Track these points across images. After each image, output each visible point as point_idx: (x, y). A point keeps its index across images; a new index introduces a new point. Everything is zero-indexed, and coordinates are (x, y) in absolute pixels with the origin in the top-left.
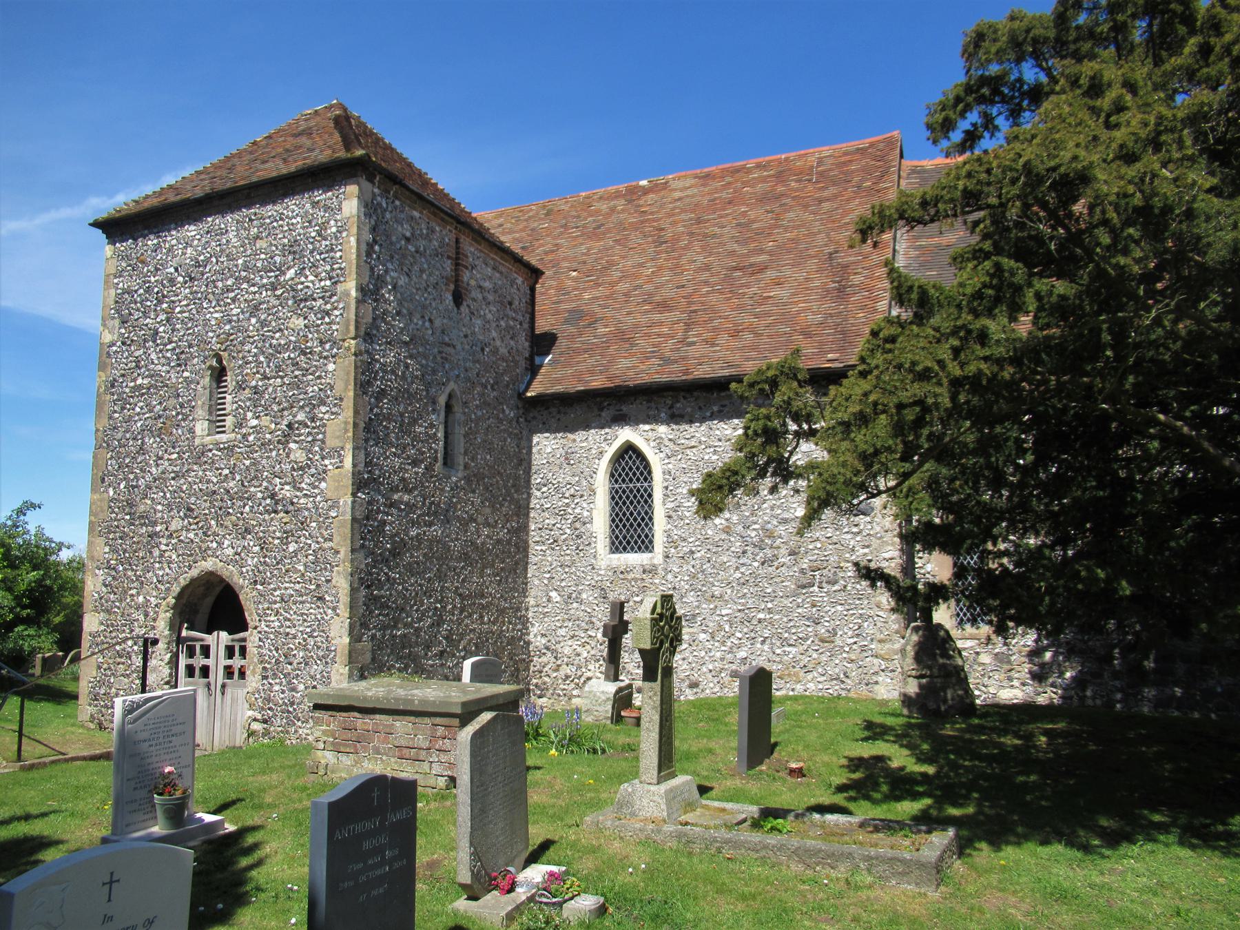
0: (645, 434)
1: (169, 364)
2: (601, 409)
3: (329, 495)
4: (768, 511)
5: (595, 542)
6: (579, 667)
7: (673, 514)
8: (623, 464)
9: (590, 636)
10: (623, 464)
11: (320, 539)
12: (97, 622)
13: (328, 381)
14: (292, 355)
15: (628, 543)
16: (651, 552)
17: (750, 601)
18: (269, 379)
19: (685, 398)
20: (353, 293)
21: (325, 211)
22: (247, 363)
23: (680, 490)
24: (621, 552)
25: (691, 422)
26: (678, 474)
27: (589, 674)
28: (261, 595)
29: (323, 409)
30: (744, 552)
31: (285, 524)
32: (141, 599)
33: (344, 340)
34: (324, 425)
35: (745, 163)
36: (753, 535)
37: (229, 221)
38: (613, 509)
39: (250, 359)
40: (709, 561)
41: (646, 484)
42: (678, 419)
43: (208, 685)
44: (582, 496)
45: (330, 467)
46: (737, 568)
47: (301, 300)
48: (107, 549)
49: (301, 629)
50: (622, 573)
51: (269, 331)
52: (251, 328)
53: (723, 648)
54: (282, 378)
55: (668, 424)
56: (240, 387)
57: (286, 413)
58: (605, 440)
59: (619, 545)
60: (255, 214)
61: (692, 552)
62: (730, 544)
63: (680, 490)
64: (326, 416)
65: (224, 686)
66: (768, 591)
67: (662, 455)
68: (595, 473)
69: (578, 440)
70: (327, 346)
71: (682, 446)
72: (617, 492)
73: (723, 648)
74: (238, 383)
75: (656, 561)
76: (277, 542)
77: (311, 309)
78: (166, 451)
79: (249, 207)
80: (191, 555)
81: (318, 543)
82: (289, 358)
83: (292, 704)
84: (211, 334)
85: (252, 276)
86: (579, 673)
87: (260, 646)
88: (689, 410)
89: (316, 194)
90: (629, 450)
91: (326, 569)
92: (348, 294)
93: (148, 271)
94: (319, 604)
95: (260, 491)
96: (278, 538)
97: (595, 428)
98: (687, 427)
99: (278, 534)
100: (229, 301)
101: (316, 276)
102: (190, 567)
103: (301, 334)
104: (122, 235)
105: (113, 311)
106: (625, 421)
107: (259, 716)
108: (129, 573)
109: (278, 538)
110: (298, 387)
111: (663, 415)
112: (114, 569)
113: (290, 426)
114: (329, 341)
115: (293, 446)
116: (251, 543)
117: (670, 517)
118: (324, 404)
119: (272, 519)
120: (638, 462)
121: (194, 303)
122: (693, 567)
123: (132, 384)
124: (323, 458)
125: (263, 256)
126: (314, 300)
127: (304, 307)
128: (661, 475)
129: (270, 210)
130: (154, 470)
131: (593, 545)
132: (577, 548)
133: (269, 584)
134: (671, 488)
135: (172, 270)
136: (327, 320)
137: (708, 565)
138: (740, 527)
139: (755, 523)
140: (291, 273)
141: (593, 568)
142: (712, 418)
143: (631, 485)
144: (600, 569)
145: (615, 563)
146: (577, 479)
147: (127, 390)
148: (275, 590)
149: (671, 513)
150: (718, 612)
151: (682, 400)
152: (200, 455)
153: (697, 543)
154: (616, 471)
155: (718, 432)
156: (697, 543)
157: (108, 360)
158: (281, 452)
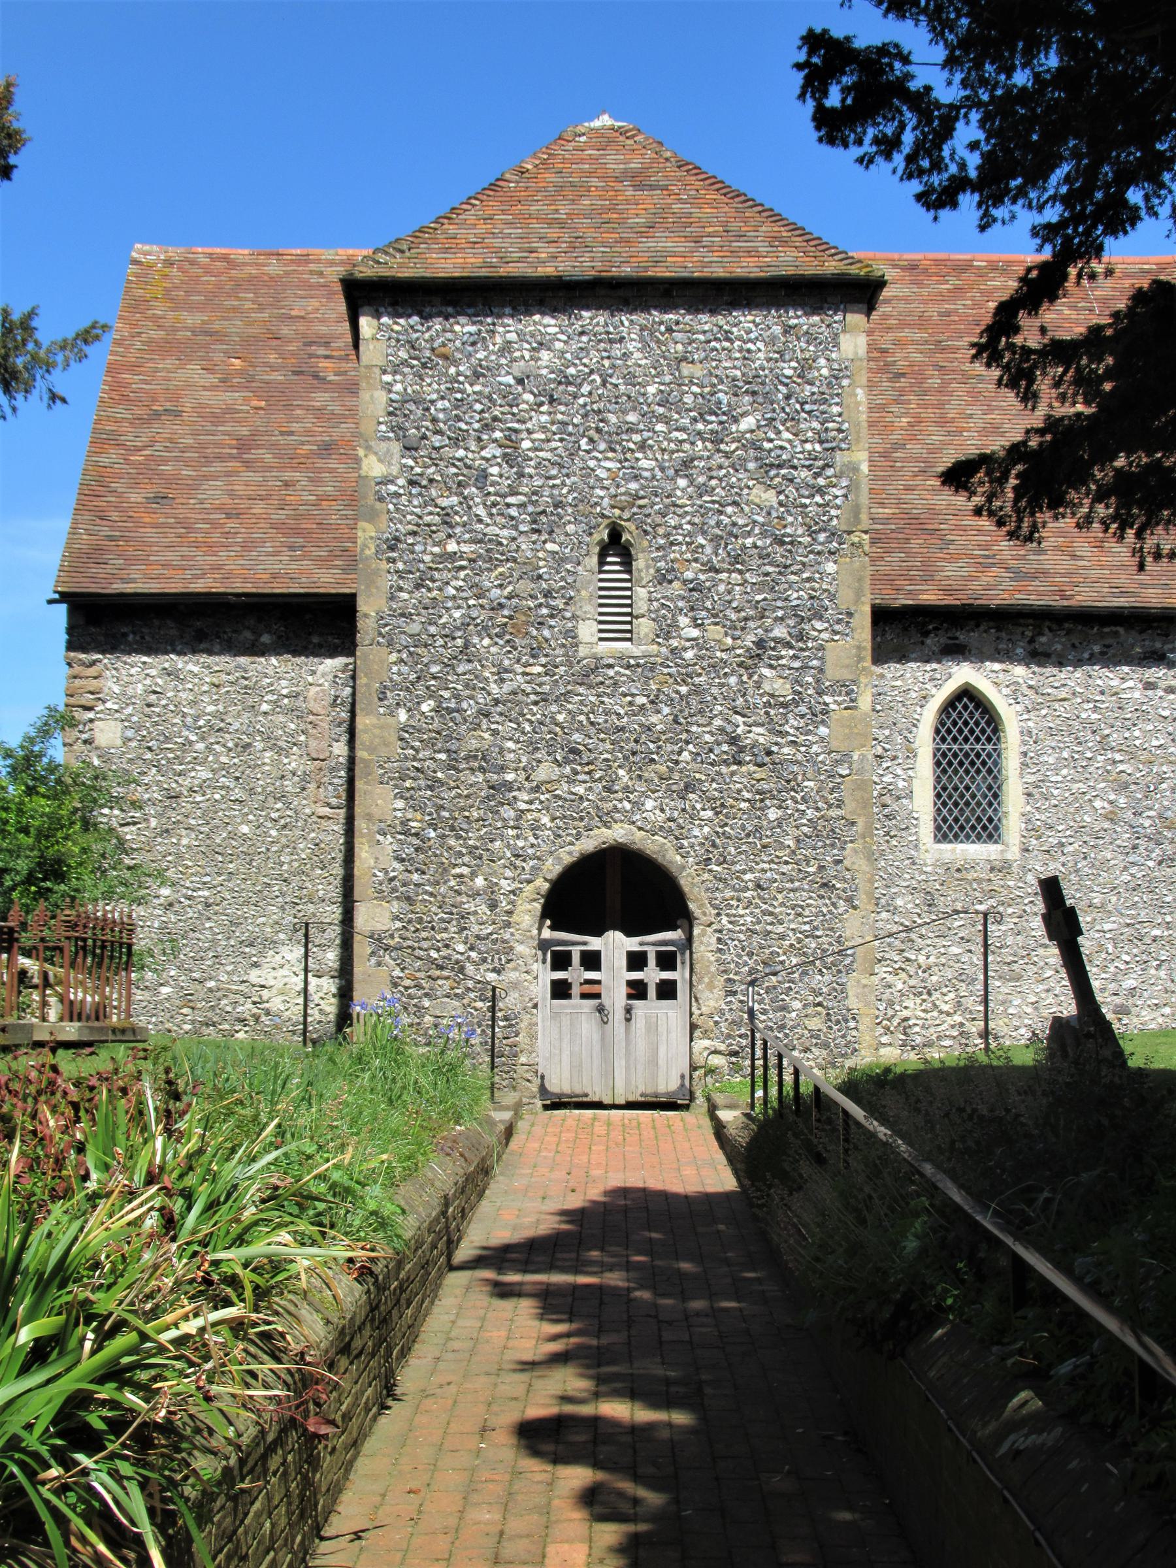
0: (994, 675)
1: (516, 528)
2: (926, 634)
3: (834, 745)
4: (1168, 793)
5: (916, 826)
6: (891, 1004)
7: (1035, 791)
8: (954, 715)
9: (908, 960)
10: (954, 715)
11: (820, 804)
12: (388, 914)
13: (825, 586)
14: (759, 543)
15: (962, 828)
16: (996, 842)
17: (1143, 914)
18: (717, 571)
19: (1051, 630)
20: (865, 468)
21: (808, 343)
22: (672, 544)
23: (1044, 758)
24: (950, 842)
25: (1060, 664)
26: (1041, 735)
27: (905, 1013)
28: (720, 880)
29: (819, 625)
30: (1135, 847)
31: (758, 781)
32: (480, 882)
33: (850, 533)
34: (821, 648)
35: (968, 257)
36: (1147, 825)
37: (628, 323)
38: (938, 780)
39: (680, 538)
40: (1085, 858)
41: (989, 747)
42: (1043, 659)
43: (601, 1009)
44: (895, 758)
45: (833, 707)
46: (1125, 869)
47: (772, 465)
48: (400, 804)
49: (792, 926)
50: (958, 870)
51: (713, 502)
52: (679, 493)
53: (1104, 976)
54: (740, 572)
55: (1027, 665)
56: (662, 579)
57: (751, 624)
58: (932, 679)
59: (946, 831)
60: (677, 323)
61: (1062, 845)
62: (1114, 836)
63: (1044, 758)
64: (825, 636)
65: (628, 1010)
66: (1168, 899)
67: (1019, 708)
68: (915, 726)
69: (889, 676)
70: (822, 537)
71: (1048, 698)
72: (944, 755)
73: (1104, 976)
74: (658, 570)
75: (1009, 856)
76: (744, 805)
77: (791, 481)
78: (518, 661)
79: (665, 309)
80: (582, 819)
81: (817, 809)
82: (755, 546)
83: (782, 1027)
84: (599, 492)
85: (676, 416)
86: (890, 1012)
87: (720, 950)
88: (1059, 647)
89: (791, 313)
90: (967, 695)
91: (833, 845)
92: (856, 469)
93: (459, 374)
94: (822, 892)
95: (710, 733)
96: (748, 800)
97: (916, 660)
98: (1055, 671)
99: (747, 795)
100: (632, 446)
101: (796, 435)
102: (578, 836)
103: (774, 514)
104: (394, 304)
105: (383, 428)
106: (963, 653)
107: (722, 1047)
108: (452, 842)
109: (748, 800)
110: (772, 589)
111: (1019, 651)
112: (416, 835)
113: (760, 644)
114: (825, 530)
115: (766, 672)
116: (698, 806)
117: (1029, 795)
118: (821, 618)
119: (733, 774)
120: (977, 715)
121: (561, 440)
122: (1063, 865)
123: (436, 550)
124: (820, 694)
125: (695, 389)
126: (795, 468)
127: (777, 475)
128: (1018, 736)
129: (706, 321)
130: (494, 688)
131: (913, 830)
132: (887, 834)
133: (733, 863)
134: (1032, 754)
135: (510, 380)
136: (818, 499)
137: (1085, 863)
138: (1129, 813)
139: (1150, 809)
140: (748, 423)
141: (914, 863)
142: (1091, 661)
143: (955, 747)
144: (925, 865)
145: (947, 857)
146: (887, 732)
147: (427, 558)
148: (744, 872)
149: (1031, 789)
150: (1098, 927)
151: (1046, 631)
152: (590, 673)
153: (1068, 833)
154: (943, 725)
155: (1099, 682)
156: (1068, 833)
157: (378, 505)
158: (745, 678)
